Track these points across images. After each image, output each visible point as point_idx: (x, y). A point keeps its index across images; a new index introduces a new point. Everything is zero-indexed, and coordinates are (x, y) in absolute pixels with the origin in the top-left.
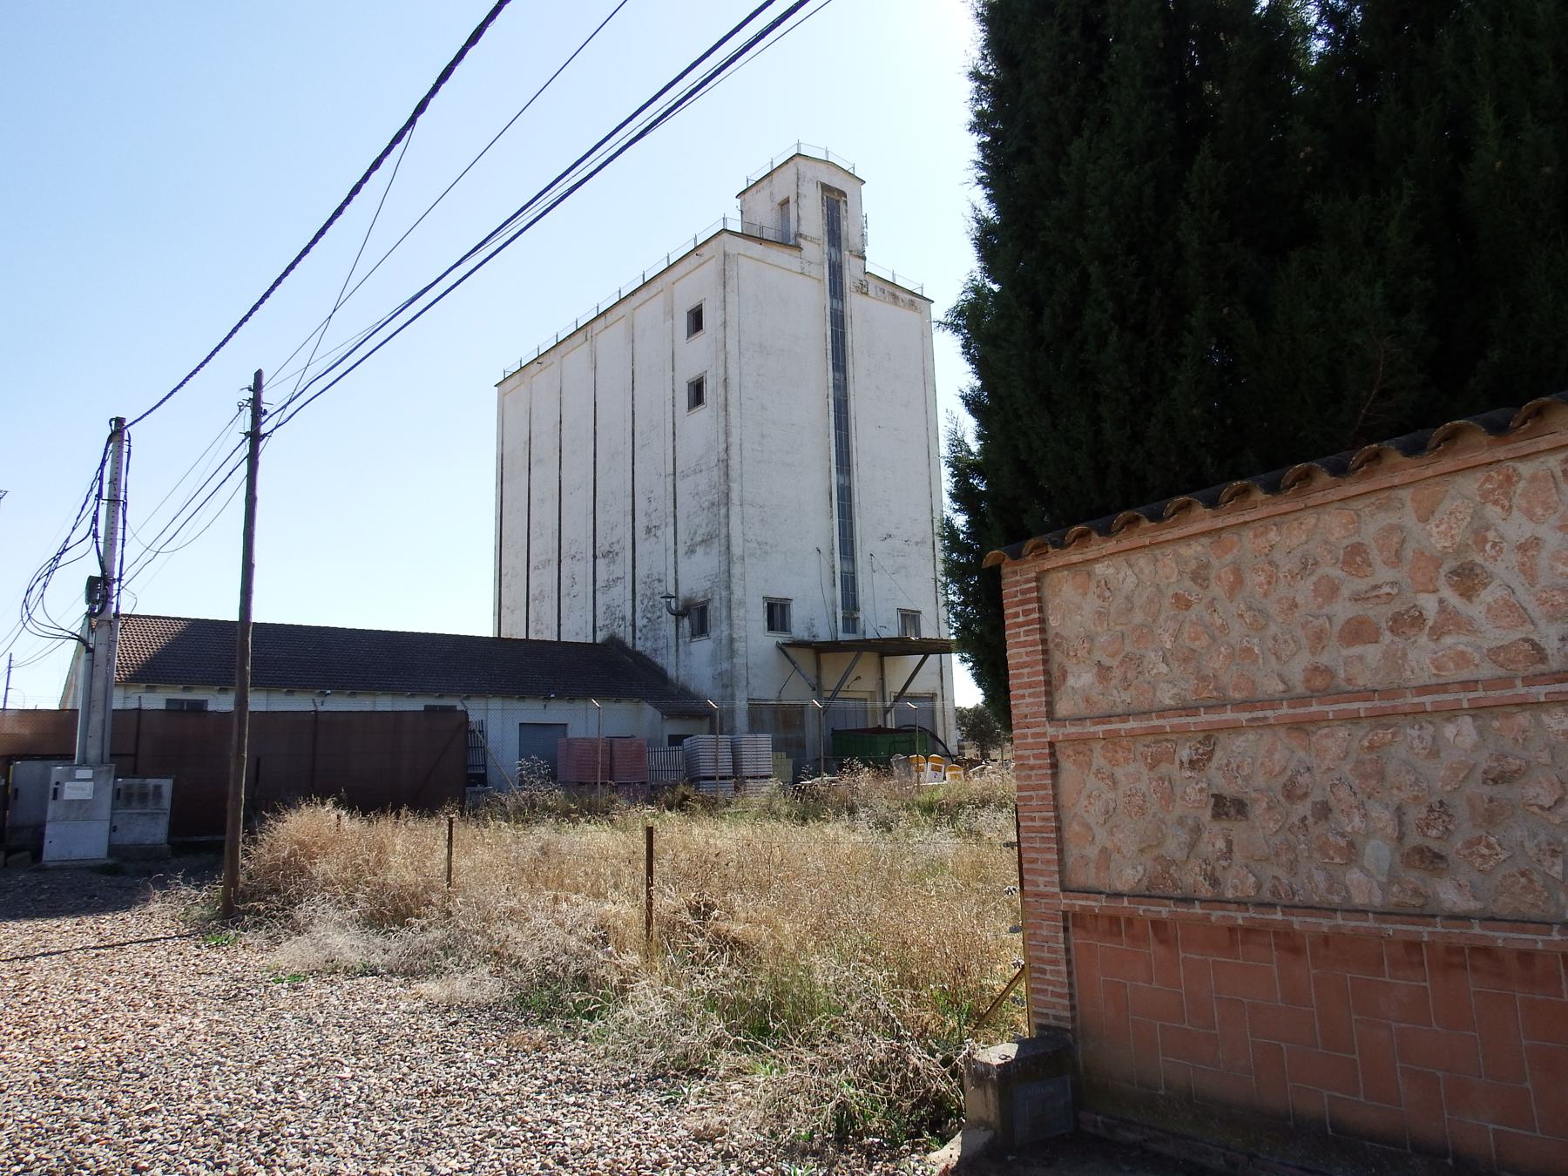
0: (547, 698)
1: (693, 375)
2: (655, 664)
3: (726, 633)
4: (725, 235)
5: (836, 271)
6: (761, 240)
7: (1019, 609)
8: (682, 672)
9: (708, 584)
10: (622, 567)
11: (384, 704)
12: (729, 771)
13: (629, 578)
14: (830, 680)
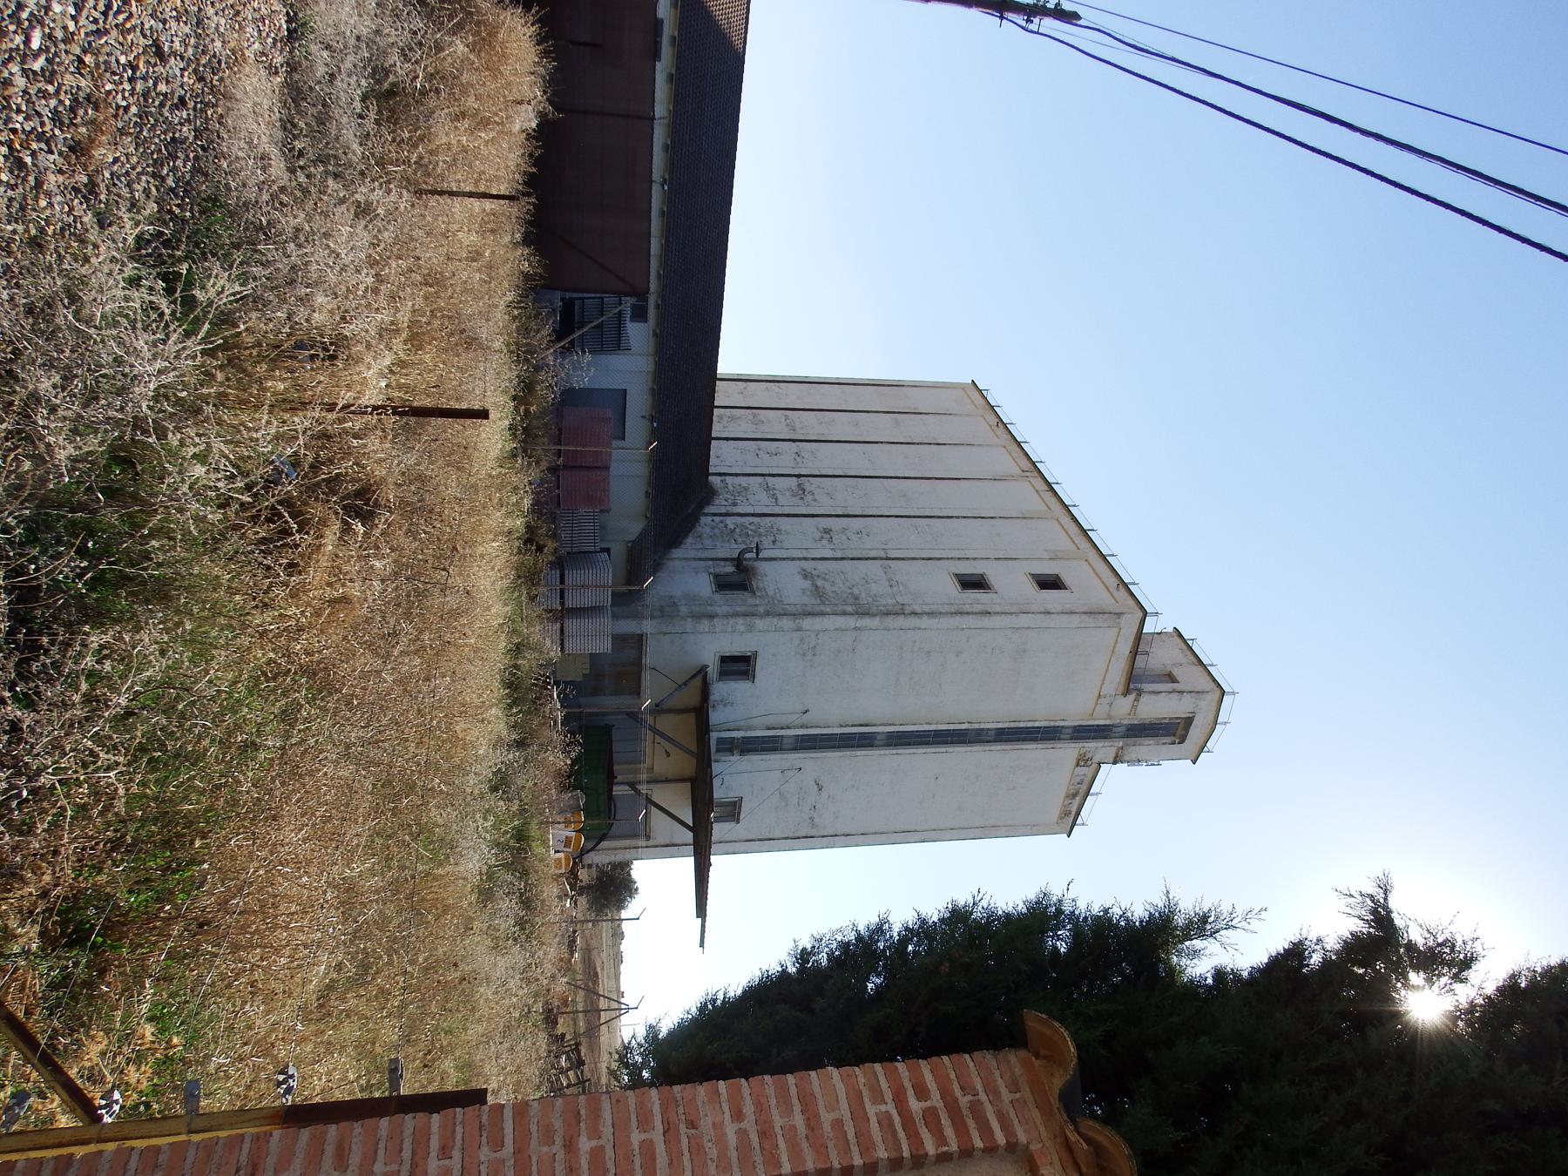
0: (652, 419)
1: (992, 579)
2: (686, 536)
3: (718, 610)
4: (1140, 614)
5: (1100, 732)
6: (1135, 652)
7: (936, 1100)
8: (677, 563)
9: (771, 593)
10: (788, 504)
11: (655, 247)
12: (569, 604)
13: (777, 510)
14: (666, 723)
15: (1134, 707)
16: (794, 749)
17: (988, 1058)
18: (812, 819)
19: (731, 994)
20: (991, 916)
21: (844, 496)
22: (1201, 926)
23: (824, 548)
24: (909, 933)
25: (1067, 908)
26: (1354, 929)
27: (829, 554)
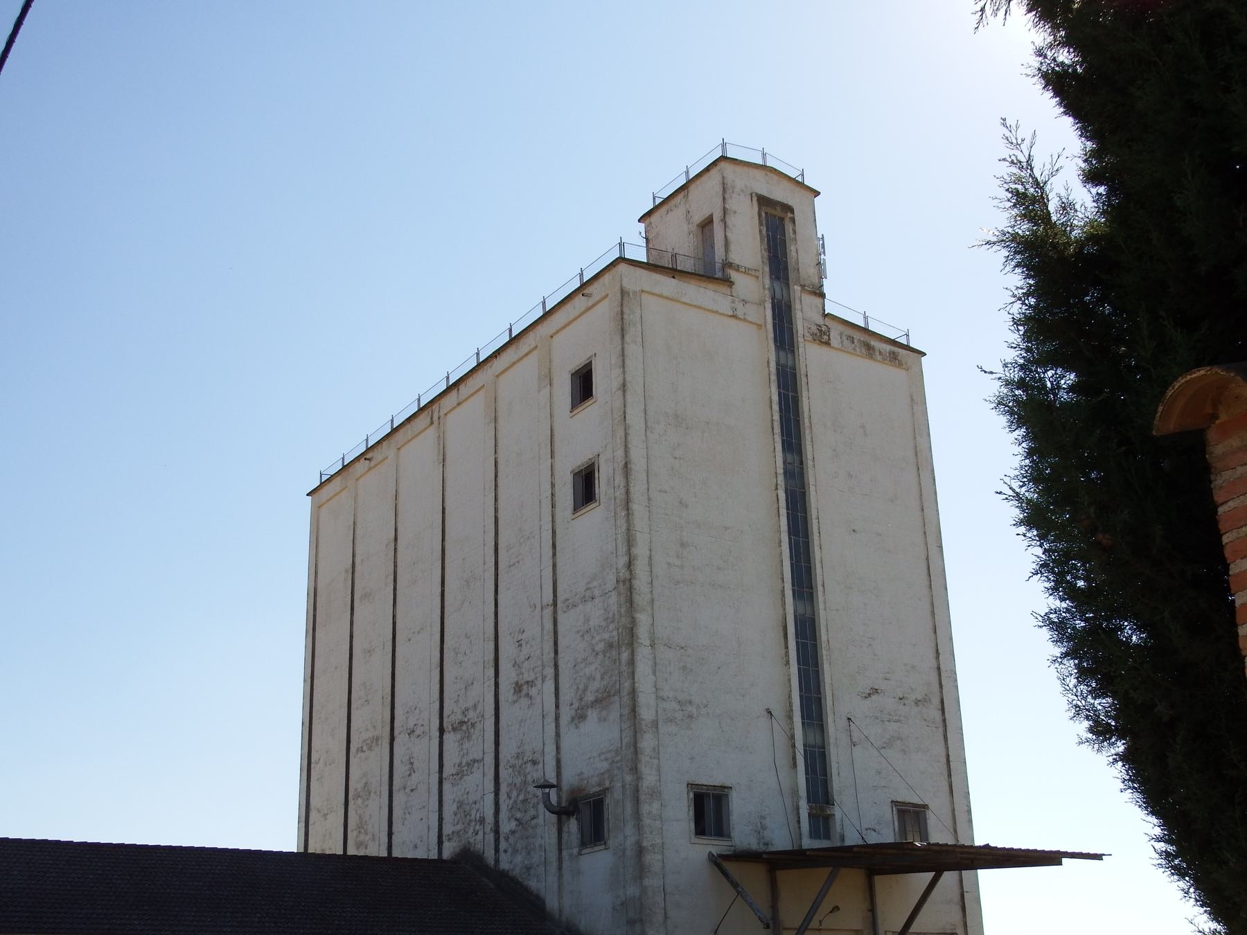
2: (527, 890)
3: (631, 841)
5: (783, 315)
6: (673, 272)
9: (606, 765)
10: (481, 744)
13: (489, 759)
15: (747, 271)
16: (822, 727)
17: (1221, 481)
18: (917, 702)
19: (1158, 831)
20: (1035, 476)
21: (469, 666)
22: (1029, 201)
23: (541, 692)
24: (1061, 586)
25: (1016, 375)
26: (1024, 9)
27: (549, 686)
